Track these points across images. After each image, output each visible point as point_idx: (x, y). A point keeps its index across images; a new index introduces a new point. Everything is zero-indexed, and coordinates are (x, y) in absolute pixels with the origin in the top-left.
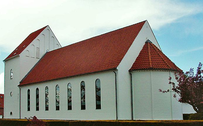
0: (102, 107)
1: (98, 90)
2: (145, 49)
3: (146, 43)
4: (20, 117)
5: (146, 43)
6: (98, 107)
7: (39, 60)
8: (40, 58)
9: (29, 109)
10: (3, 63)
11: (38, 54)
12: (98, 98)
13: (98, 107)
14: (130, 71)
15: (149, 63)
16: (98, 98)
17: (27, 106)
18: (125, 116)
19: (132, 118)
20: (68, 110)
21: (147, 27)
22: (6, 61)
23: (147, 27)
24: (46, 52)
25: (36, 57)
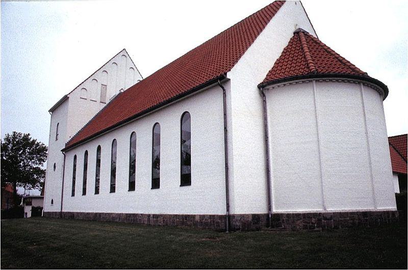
0: (77, 191)
1: (185, 138)
2: (288, 53)
3: (294, 33)
4: (61, 209)
5: (297, 33)
6: (186, 180)
7: (105, 105)
8: (107, 103)
9: (73, 195)
10: (49, 115)
11: (103, 95)
12: (186, 160)
13: (186, 180)
14: (263, 88)
15: (308, 65)
16: (186, 160)
17: (88, 185)
18: (248, 202)
19: (270, 208)
20: (95, 194)
21: (296, 4)
22: (53, 110)
23: (296, 4)
24: (118, 92)
25: (99, 101)
